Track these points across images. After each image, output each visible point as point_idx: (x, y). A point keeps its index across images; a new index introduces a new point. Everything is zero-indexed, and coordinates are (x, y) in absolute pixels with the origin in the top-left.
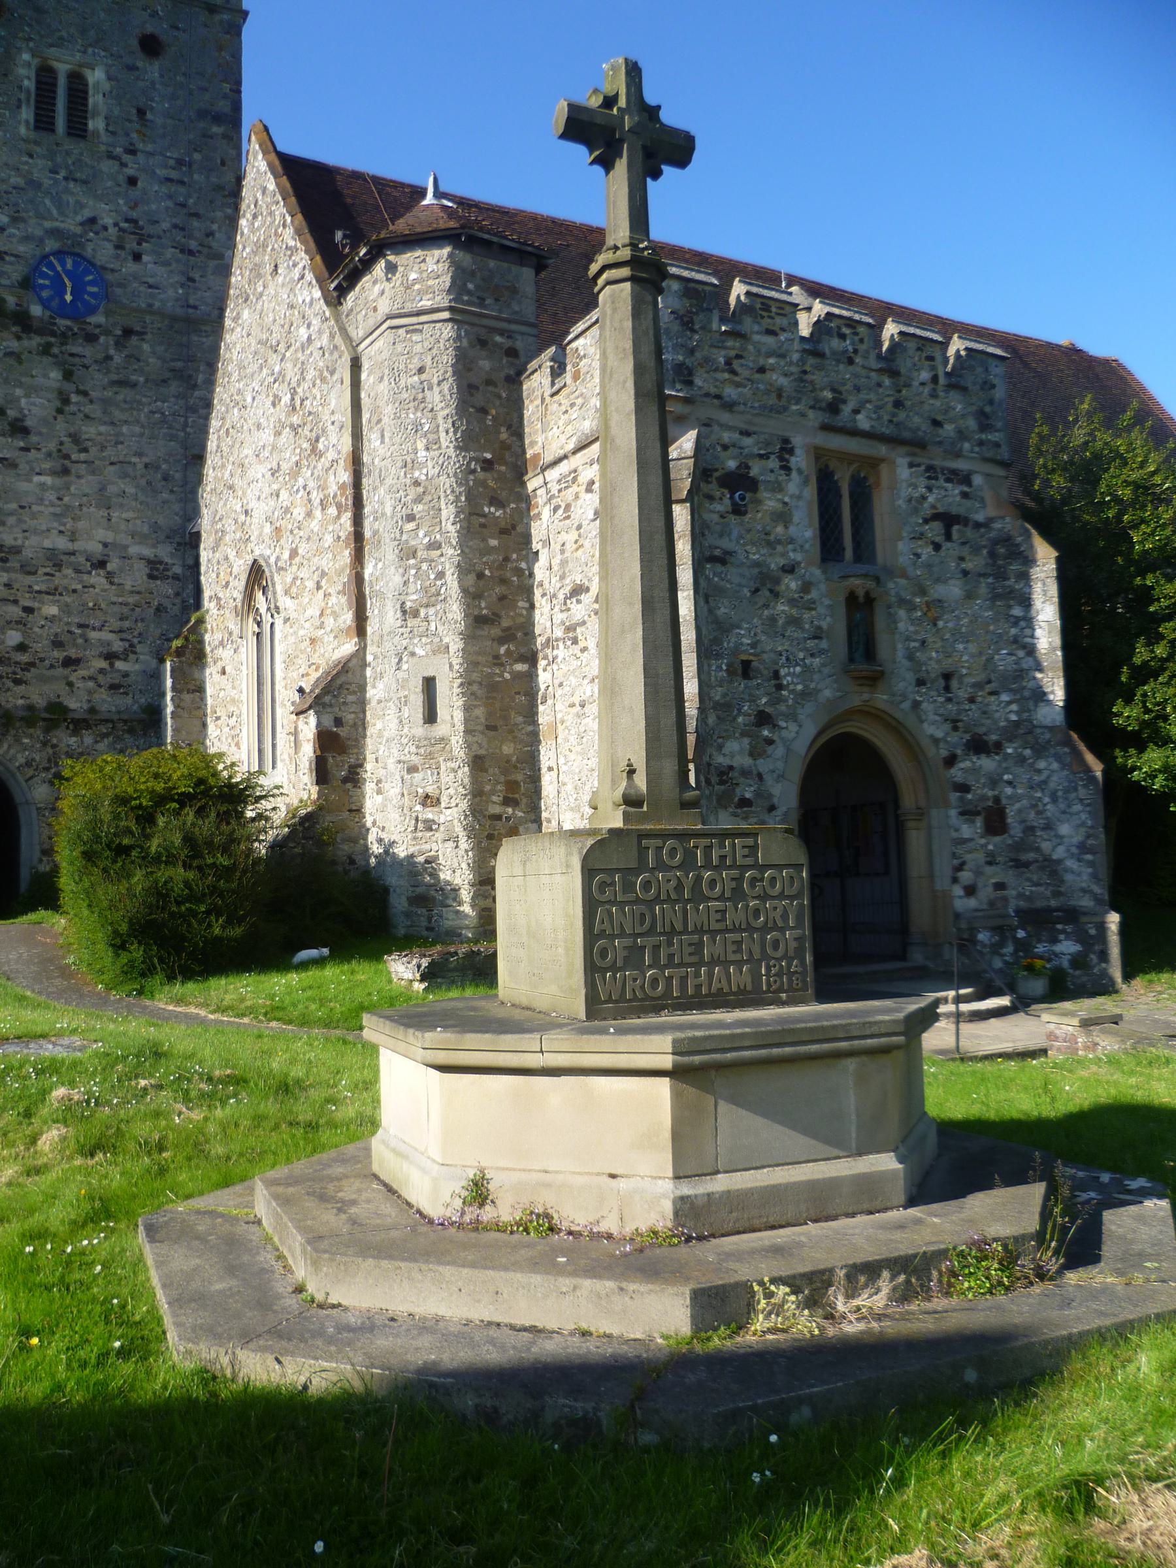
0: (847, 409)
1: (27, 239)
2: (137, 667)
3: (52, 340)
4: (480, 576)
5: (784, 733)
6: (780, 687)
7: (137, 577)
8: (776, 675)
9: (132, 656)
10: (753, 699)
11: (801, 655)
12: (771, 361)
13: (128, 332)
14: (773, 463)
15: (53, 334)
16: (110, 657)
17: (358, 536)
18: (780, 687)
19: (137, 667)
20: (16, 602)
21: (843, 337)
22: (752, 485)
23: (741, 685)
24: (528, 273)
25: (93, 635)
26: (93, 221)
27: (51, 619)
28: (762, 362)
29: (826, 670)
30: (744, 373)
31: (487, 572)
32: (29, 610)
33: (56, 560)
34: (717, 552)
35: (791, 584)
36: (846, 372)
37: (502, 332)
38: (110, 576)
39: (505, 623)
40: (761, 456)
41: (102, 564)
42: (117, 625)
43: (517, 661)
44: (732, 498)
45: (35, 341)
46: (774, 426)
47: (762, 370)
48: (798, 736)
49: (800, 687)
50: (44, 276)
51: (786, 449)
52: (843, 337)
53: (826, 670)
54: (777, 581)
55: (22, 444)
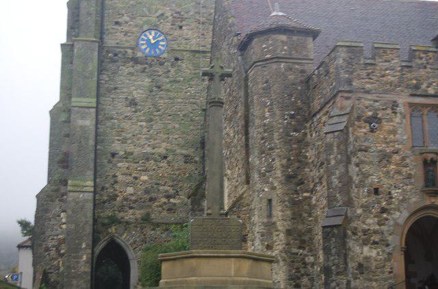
0: (424, 86)
1: (136, 26)
2: (179, 201)
3: (146, 66)
4: (289, 160)
5: (393, 216)
6: (391, 198)
7: (180, 163)
8: (390, 193)
9: (177, 197)
10: (379, 203)
11: (401, 185)
12: (387, 72)
13: (177, 59)
14: (389, 111)
15: (147, 64)
16: (168, 197)
17: (247, 146)
18: (391, 198)
19: (179, 201)
20: (130, 175)
21: (421, 58)
22: (379, 121)
23: (373, 198)
24: (310, 39)
25: (161, 188)
26: (162, 15)
27: (145, 182)
28: (383, 73)
29: (413, 191)
30: (375, 78)
31: (292, 158)
32: (136, 178)
33: (147, 158)
34: (363, 148)
35: (396, 157)
36: (422, 72)
37: (298, 64)
38: (169, 163)
39: (300, 177)
40: (383, 109)
41: (165, 157)
42: (171, 184)
43: (305, 192)
44: (370, 126)
45: (139, 67)
46: (390, 97)
47: (383, 76)
48: (401, 217)
49: (401, 198)
50: (143, 40)
51: (395, 105)
52: (421, 58)
53: (413, 191)
54: (391, 157)
55: (134, 110)
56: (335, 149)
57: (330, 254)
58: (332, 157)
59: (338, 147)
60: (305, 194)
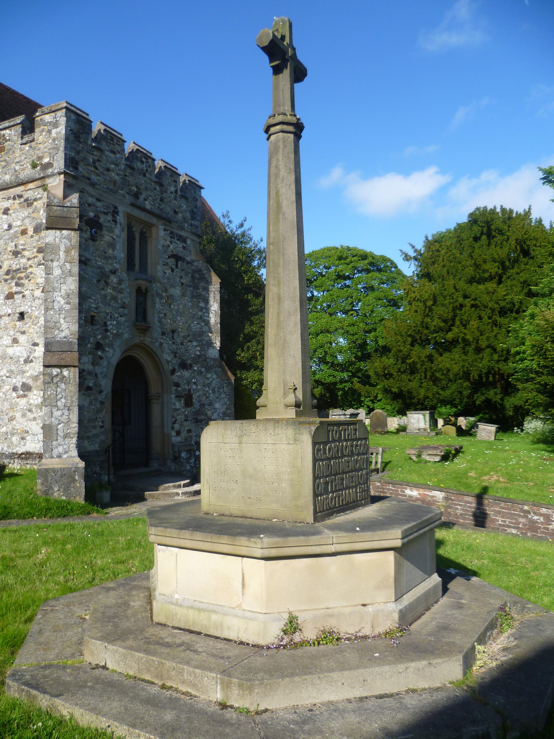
6: (107, 331)
8: (105, 324)
18: (107, 331)
30: (101, 169)
56: (62, 253)
57: (56, 406)
58: (55, 264)
59: (67, 251)
60: (532, 376)
